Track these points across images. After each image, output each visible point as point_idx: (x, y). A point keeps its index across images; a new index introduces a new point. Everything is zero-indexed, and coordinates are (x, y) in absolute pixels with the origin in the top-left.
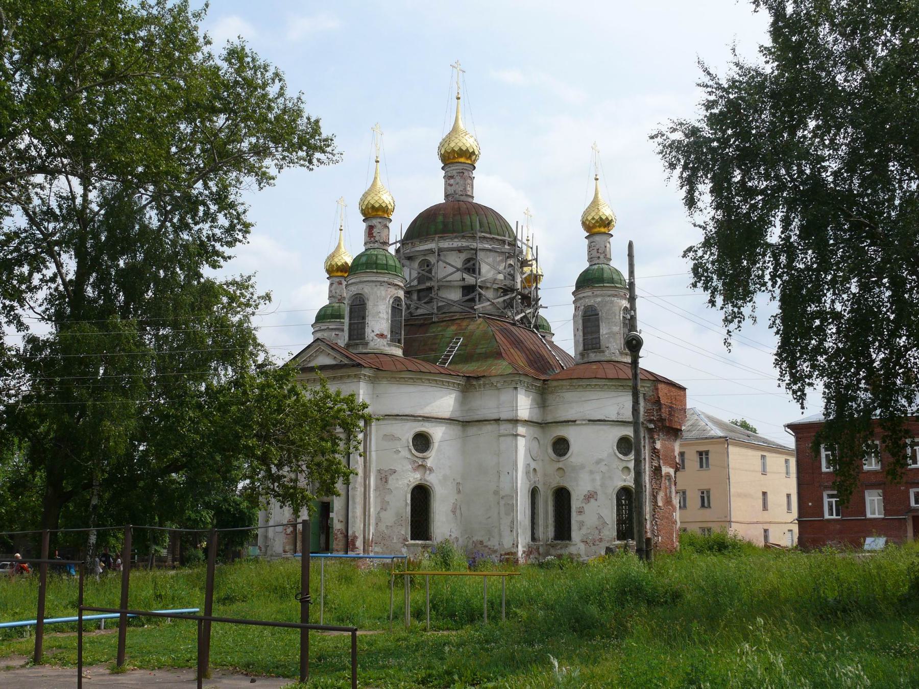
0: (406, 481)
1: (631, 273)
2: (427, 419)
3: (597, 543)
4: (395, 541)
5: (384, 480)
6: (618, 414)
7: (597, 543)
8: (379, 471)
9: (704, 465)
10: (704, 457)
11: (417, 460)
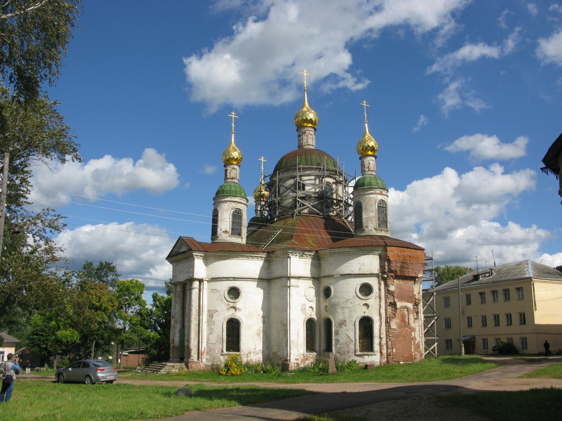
0: (223, 317)
1: (269, 176)
2: (235, 279)
3: (346, 353)
4: (217, 352)
5: (211, 316)
6: (360, 269)
7: (346, 353)
8: (209, 311)
9: (496, 300)
10: (507, 292)
11: (229, 303)
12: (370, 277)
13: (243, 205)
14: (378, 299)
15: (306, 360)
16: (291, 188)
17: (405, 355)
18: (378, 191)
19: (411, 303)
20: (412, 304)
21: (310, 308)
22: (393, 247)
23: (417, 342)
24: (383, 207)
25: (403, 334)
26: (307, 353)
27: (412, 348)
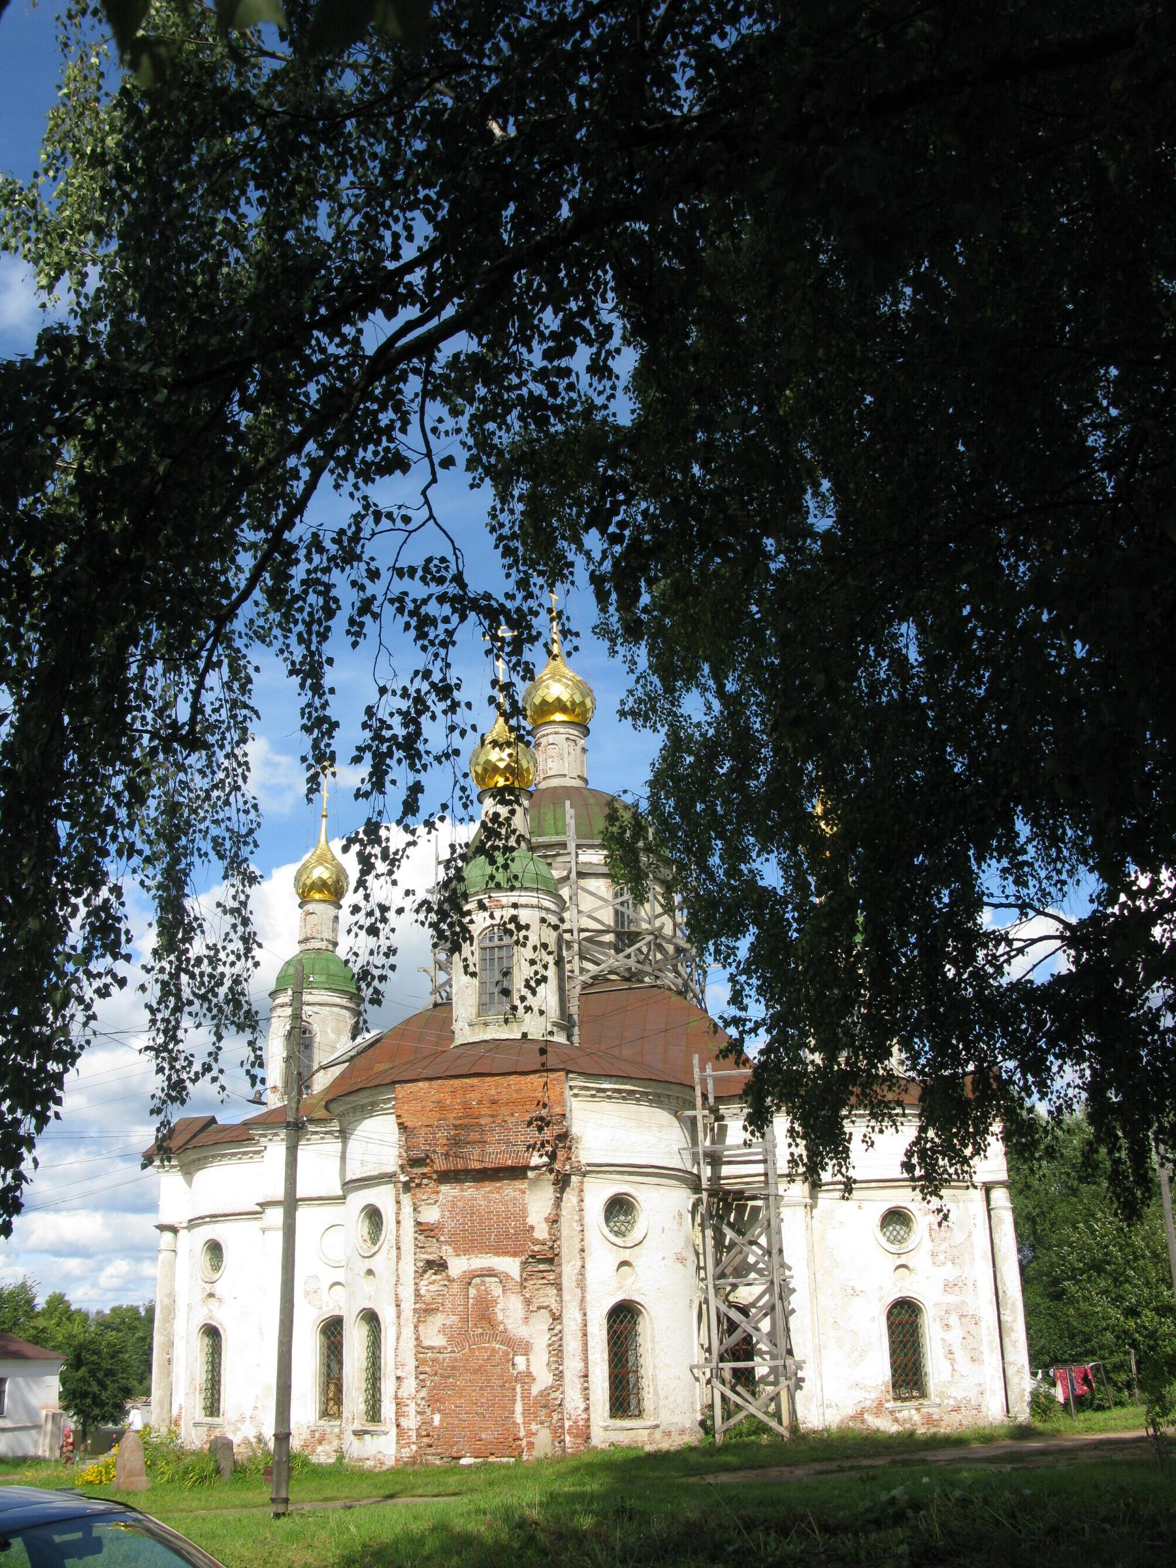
2: (214, 1218)
12: (378, 1184)
14: (394, 1252)
15: (320, 1442)
19: (515, 1254)
21: (624, 1268)
22: (421, 1084)
23: (535, 1390)
24: (500, 947)
25: (473, 1364)
26: (322, 1422)
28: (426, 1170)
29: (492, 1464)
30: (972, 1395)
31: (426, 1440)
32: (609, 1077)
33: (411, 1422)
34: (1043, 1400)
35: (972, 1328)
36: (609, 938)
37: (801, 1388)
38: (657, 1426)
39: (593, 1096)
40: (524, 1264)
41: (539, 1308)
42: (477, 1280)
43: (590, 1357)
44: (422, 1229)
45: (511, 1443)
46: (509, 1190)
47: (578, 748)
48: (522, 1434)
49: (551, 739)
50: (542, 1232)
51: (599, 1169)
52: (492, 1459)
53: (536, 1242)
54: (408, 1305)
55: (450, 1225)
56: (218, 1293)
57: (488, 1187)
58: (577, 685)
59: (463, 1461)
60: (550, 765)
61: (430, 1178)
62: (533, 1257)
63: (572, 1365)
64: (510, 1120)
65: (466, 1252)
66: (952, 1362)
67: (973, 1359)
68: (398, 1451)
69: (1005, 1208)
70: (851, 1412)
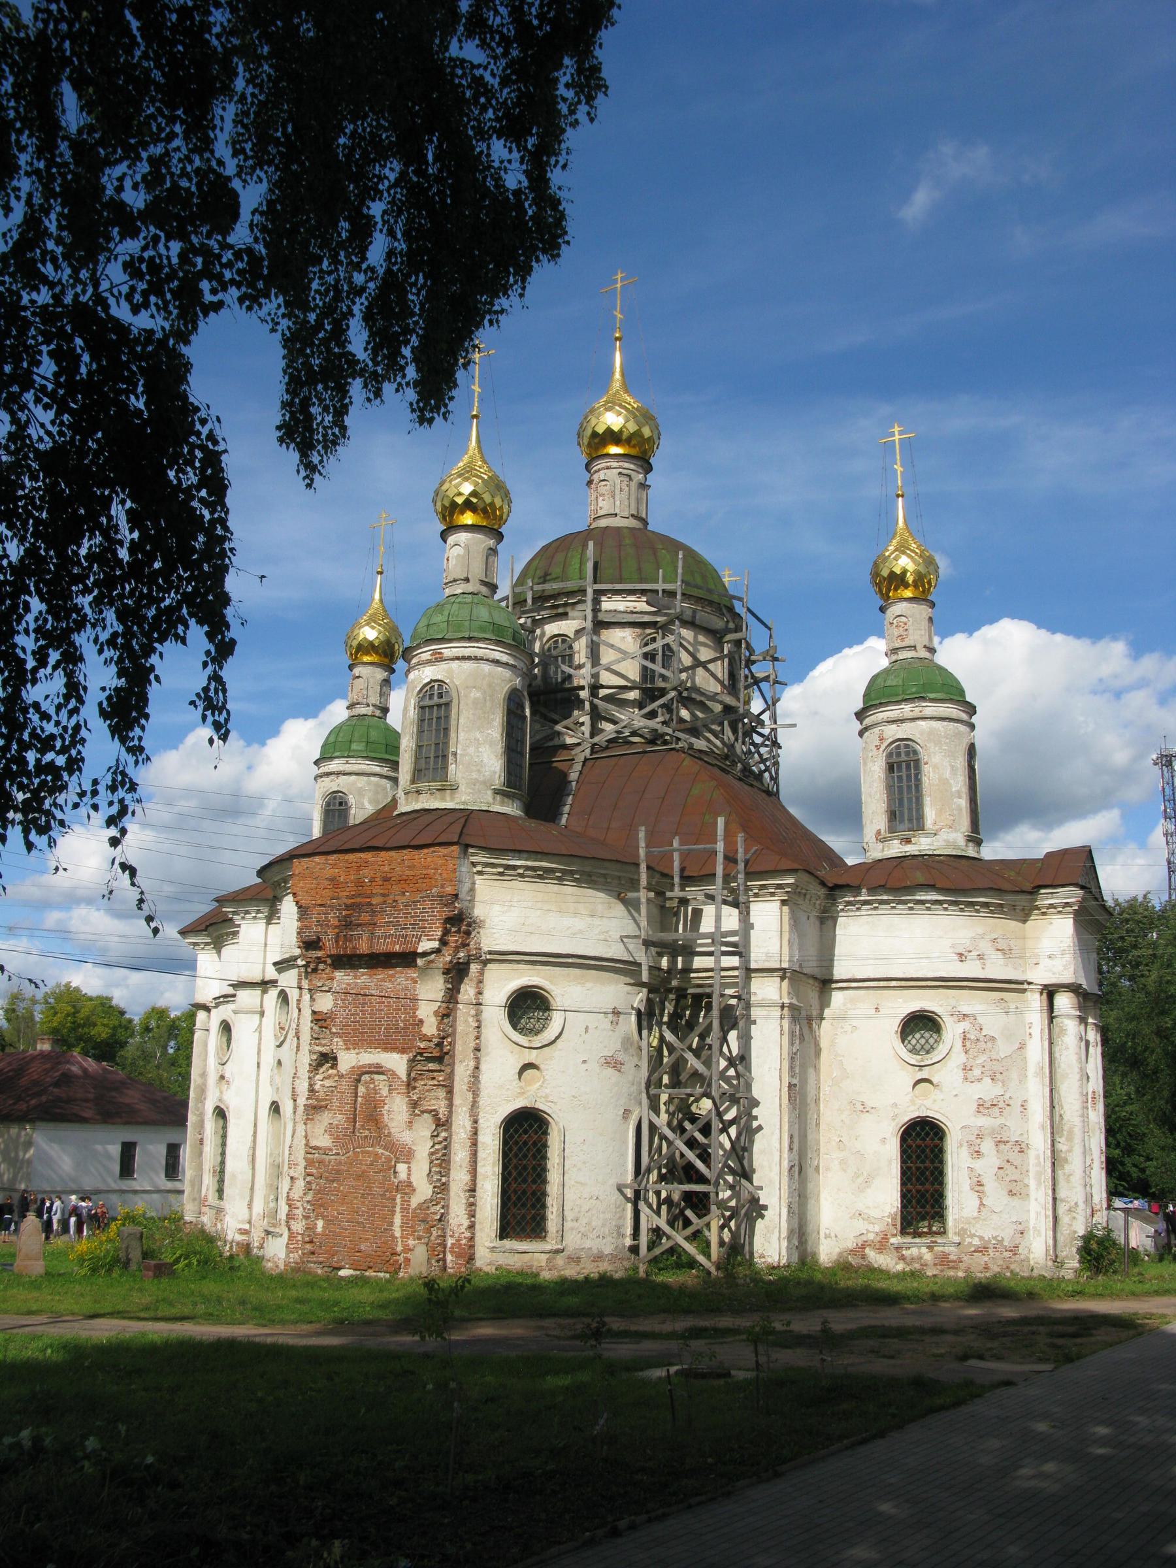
13: (353, 778)
16: (710, 666)
17: (363, 1248)
18: (425, 654)
19: (403, 1051)
20: (405, 1057)
22: (317, 859)
27: (392, 1224)
28: (320, 954)
29: (369, 1277)
30: (1007, 1235)
31: (308, 1246)
32: (518, 852)
33: (298, 1226)
34: (1095, 1246)
35: (1015, 1157)
36: (633, 695)
37: (763, 1217)
38: (558, 1251)
39: (501, 874)
40: (412, 1062)
41: (423, 1112)
42: (366, 1078)
43: (479, 1169)
44: (320, 1019)
45: (389, 1259)
46: (401, 978)
47: (634, 485)
48: (399, 1249)
49: (601, 475)
50: (430, 1028)
51: (503, 957)
52: (369, 1273)
53: (424, 1038)
54: (302, 1101)
55: (342, 1015)
56: (227, 1075)
57: (381, 974)
58: (632, 413)
59: (342, 1273)
60: (601, 504)
61: (325, 962)
62: (421, 1054)
63: (459, 1177)
64: (402, 900)
65: (356, 1046)
66: (981, 1195)
67: (1011, 1193)
68: (287, 1255)
69: (1068, 1016)
70: (850, 1244)
